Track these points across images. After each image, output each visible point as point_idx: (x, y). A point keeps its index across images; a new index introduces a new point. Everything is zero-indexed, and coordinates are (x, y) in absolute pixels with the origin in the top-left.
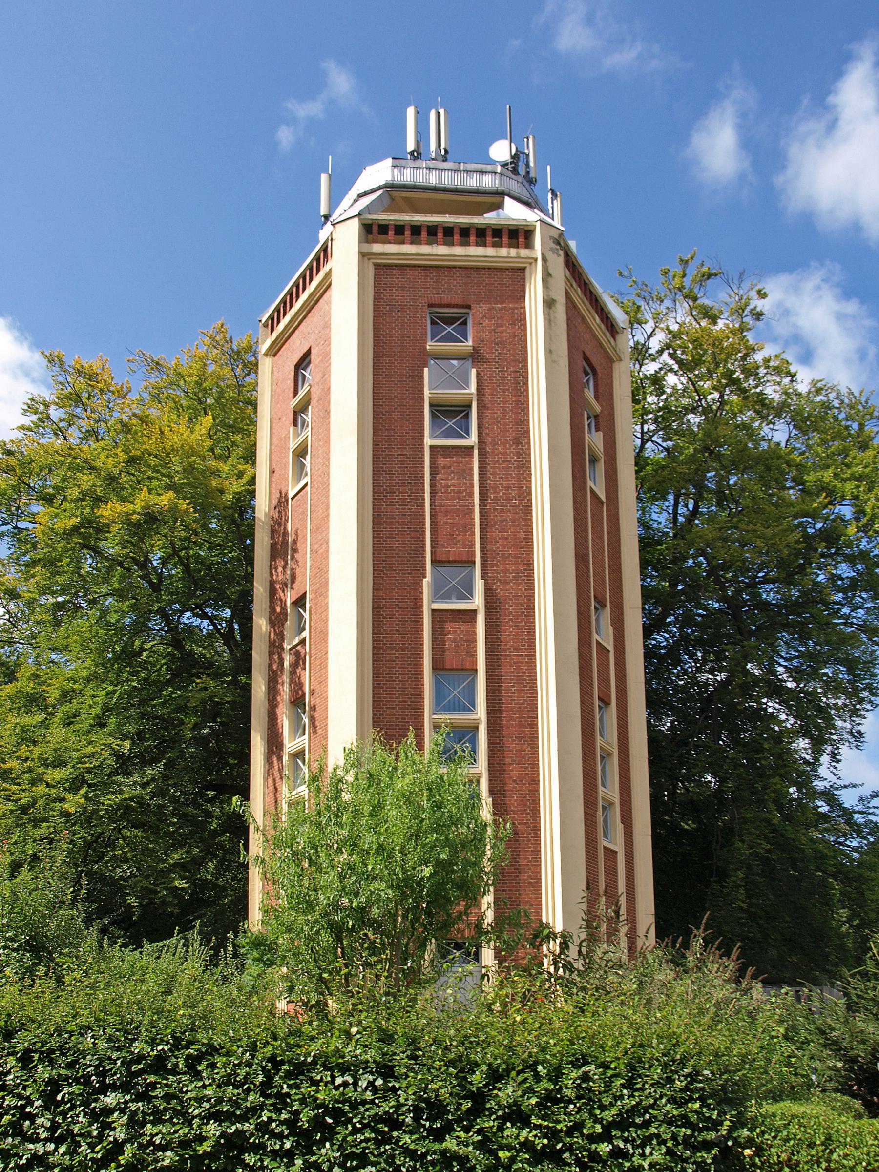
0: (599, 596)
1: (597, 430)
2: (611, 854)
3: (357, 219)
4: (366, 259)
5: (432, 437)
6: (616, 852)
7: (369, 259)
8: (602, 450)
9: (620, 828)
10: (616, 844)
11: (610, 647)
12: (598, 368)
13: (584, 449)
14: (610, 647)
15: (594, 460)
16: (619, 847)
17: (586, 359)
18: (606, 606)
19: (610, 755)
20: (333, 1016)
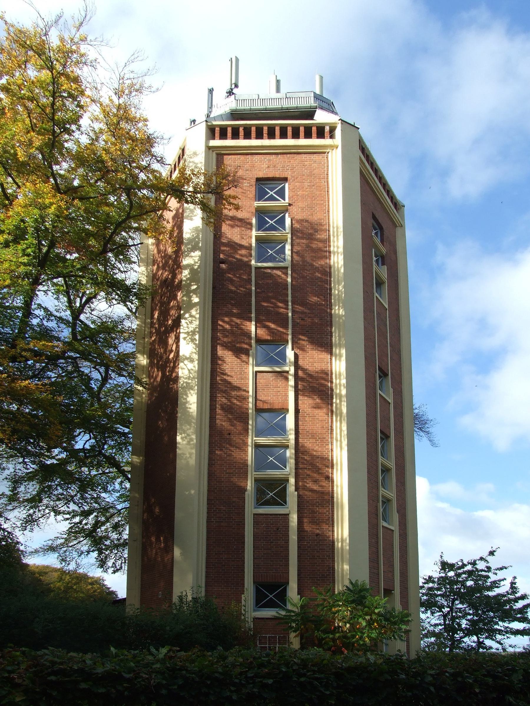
0: (386, 431)
1: (383, 264)
2: (389, 532)
3: (300, 397)
4: (211, 151)
5: (258, 261)
6: (393, 531)
7: (213, 151)
8: (386, 277)
9: (396, 517)
10: (393, 526)
11: (391, 400)
12: (384, 227)
13: (372, 273)
14: (391, 400)
15: (380, 284)
16: (395, 527)
17: (374, 217)
18: (388, 375)
19: (383, 283)
20: (118, 540)
